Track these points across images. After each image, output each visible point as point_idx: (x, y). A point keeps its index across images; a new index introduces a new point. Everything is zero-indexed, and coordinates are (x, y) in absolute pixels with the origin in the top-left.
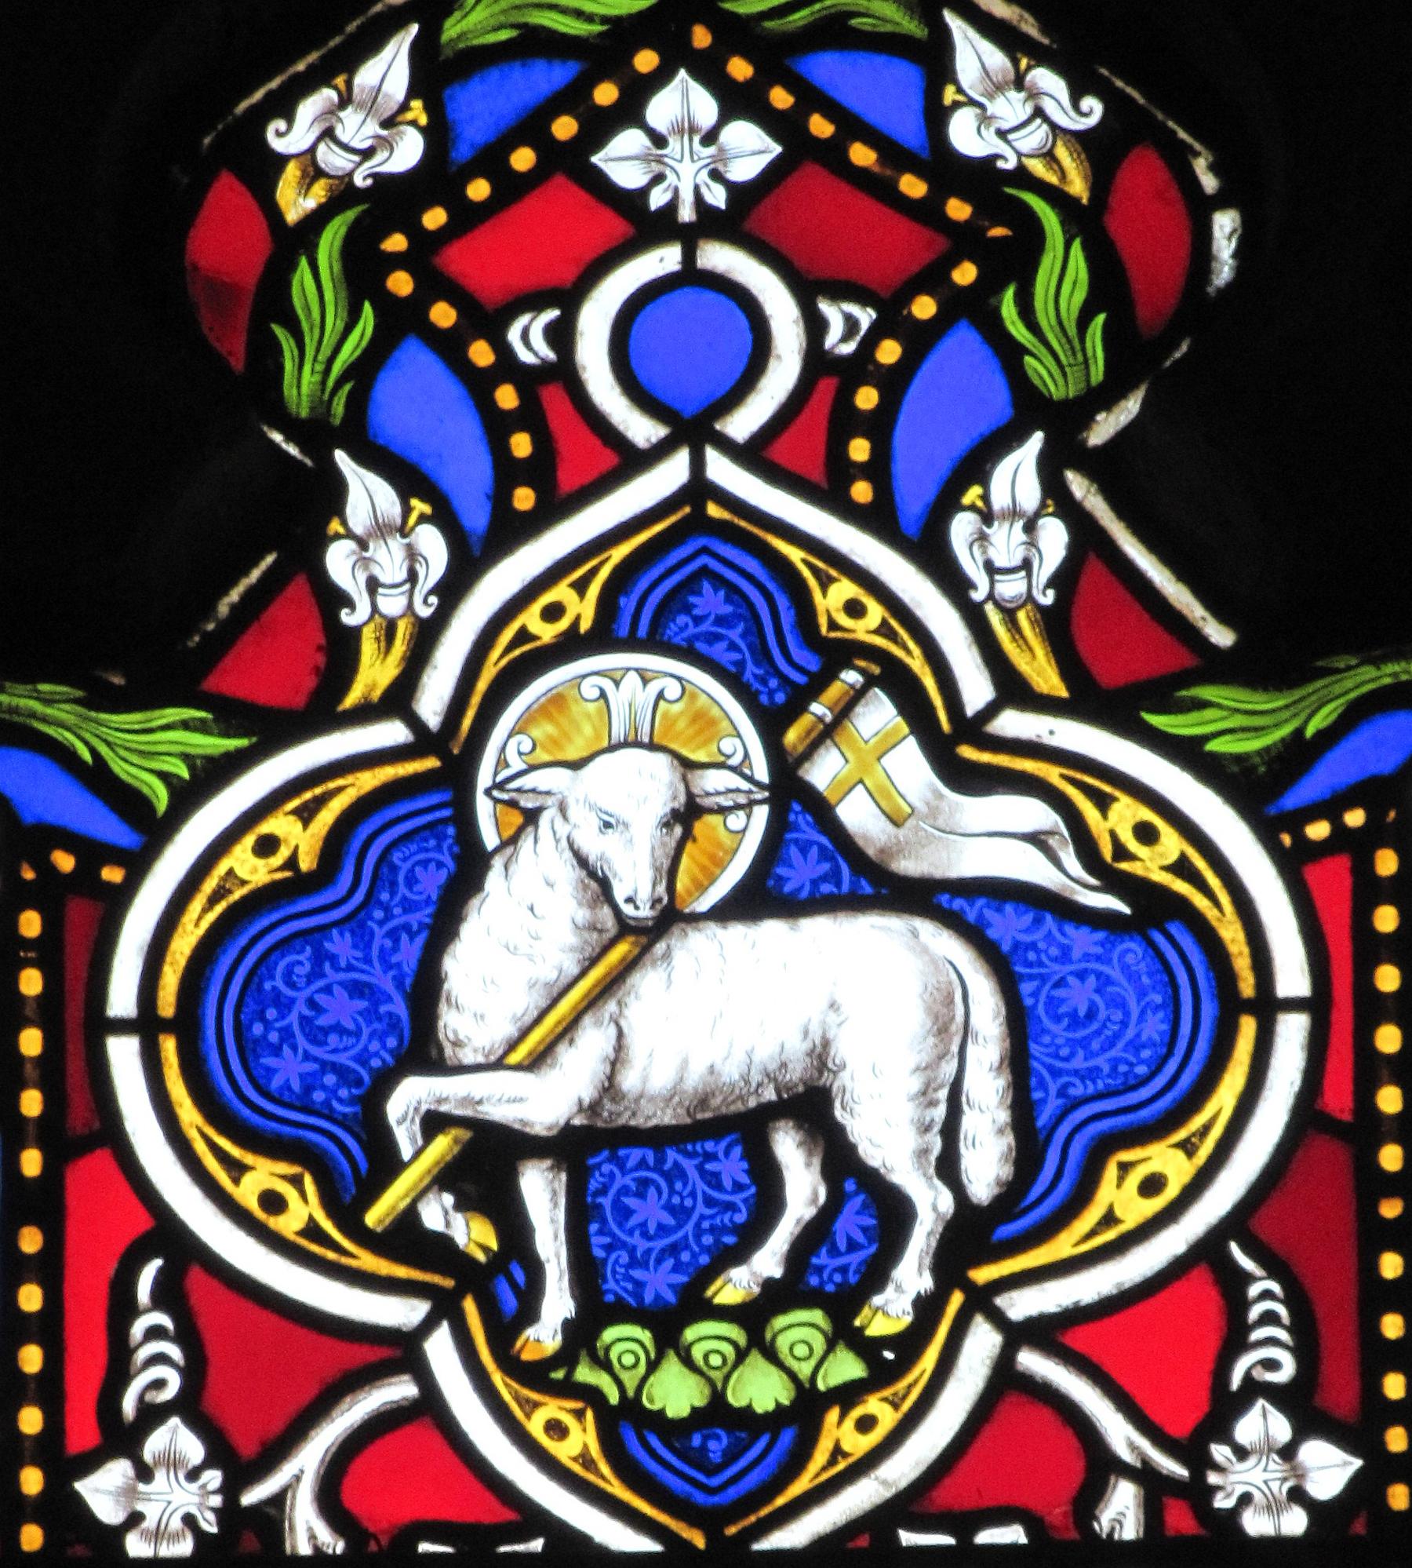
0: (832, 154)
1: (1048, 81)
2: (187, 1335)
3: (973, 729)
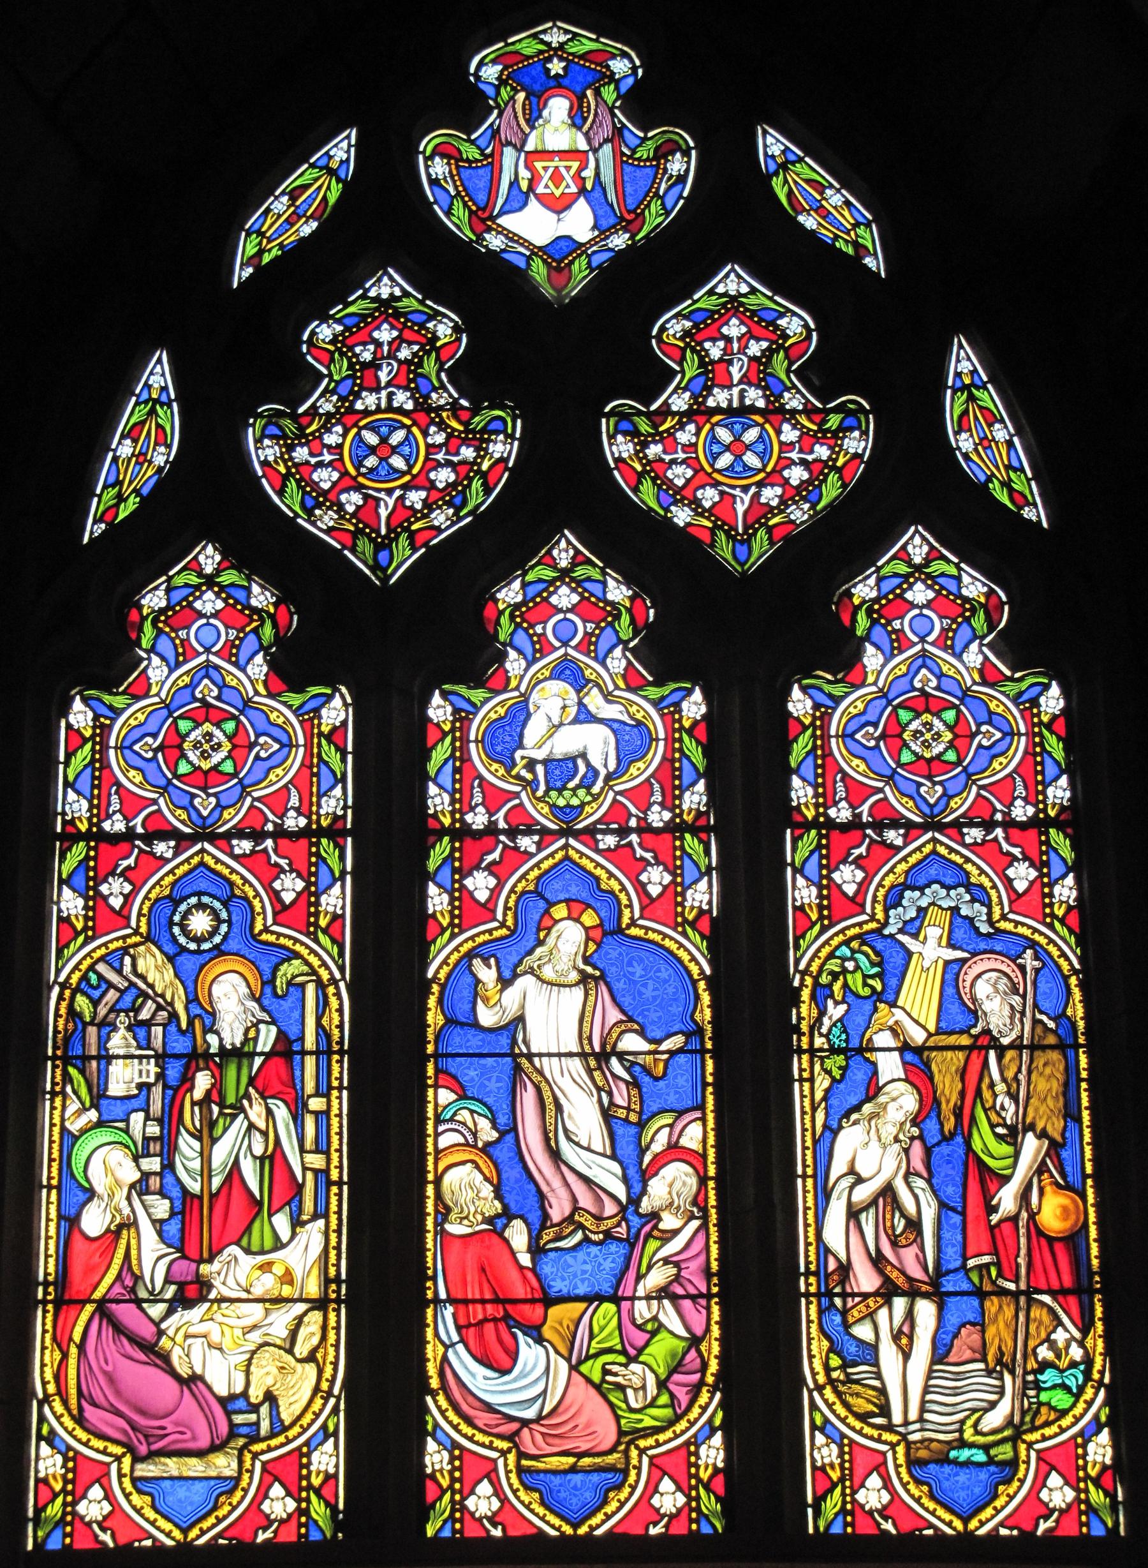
0: (588, 599)
1: (623, 588)
2: (845, 786)
3: (610, 694)
